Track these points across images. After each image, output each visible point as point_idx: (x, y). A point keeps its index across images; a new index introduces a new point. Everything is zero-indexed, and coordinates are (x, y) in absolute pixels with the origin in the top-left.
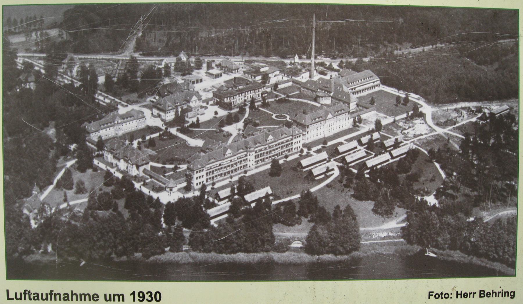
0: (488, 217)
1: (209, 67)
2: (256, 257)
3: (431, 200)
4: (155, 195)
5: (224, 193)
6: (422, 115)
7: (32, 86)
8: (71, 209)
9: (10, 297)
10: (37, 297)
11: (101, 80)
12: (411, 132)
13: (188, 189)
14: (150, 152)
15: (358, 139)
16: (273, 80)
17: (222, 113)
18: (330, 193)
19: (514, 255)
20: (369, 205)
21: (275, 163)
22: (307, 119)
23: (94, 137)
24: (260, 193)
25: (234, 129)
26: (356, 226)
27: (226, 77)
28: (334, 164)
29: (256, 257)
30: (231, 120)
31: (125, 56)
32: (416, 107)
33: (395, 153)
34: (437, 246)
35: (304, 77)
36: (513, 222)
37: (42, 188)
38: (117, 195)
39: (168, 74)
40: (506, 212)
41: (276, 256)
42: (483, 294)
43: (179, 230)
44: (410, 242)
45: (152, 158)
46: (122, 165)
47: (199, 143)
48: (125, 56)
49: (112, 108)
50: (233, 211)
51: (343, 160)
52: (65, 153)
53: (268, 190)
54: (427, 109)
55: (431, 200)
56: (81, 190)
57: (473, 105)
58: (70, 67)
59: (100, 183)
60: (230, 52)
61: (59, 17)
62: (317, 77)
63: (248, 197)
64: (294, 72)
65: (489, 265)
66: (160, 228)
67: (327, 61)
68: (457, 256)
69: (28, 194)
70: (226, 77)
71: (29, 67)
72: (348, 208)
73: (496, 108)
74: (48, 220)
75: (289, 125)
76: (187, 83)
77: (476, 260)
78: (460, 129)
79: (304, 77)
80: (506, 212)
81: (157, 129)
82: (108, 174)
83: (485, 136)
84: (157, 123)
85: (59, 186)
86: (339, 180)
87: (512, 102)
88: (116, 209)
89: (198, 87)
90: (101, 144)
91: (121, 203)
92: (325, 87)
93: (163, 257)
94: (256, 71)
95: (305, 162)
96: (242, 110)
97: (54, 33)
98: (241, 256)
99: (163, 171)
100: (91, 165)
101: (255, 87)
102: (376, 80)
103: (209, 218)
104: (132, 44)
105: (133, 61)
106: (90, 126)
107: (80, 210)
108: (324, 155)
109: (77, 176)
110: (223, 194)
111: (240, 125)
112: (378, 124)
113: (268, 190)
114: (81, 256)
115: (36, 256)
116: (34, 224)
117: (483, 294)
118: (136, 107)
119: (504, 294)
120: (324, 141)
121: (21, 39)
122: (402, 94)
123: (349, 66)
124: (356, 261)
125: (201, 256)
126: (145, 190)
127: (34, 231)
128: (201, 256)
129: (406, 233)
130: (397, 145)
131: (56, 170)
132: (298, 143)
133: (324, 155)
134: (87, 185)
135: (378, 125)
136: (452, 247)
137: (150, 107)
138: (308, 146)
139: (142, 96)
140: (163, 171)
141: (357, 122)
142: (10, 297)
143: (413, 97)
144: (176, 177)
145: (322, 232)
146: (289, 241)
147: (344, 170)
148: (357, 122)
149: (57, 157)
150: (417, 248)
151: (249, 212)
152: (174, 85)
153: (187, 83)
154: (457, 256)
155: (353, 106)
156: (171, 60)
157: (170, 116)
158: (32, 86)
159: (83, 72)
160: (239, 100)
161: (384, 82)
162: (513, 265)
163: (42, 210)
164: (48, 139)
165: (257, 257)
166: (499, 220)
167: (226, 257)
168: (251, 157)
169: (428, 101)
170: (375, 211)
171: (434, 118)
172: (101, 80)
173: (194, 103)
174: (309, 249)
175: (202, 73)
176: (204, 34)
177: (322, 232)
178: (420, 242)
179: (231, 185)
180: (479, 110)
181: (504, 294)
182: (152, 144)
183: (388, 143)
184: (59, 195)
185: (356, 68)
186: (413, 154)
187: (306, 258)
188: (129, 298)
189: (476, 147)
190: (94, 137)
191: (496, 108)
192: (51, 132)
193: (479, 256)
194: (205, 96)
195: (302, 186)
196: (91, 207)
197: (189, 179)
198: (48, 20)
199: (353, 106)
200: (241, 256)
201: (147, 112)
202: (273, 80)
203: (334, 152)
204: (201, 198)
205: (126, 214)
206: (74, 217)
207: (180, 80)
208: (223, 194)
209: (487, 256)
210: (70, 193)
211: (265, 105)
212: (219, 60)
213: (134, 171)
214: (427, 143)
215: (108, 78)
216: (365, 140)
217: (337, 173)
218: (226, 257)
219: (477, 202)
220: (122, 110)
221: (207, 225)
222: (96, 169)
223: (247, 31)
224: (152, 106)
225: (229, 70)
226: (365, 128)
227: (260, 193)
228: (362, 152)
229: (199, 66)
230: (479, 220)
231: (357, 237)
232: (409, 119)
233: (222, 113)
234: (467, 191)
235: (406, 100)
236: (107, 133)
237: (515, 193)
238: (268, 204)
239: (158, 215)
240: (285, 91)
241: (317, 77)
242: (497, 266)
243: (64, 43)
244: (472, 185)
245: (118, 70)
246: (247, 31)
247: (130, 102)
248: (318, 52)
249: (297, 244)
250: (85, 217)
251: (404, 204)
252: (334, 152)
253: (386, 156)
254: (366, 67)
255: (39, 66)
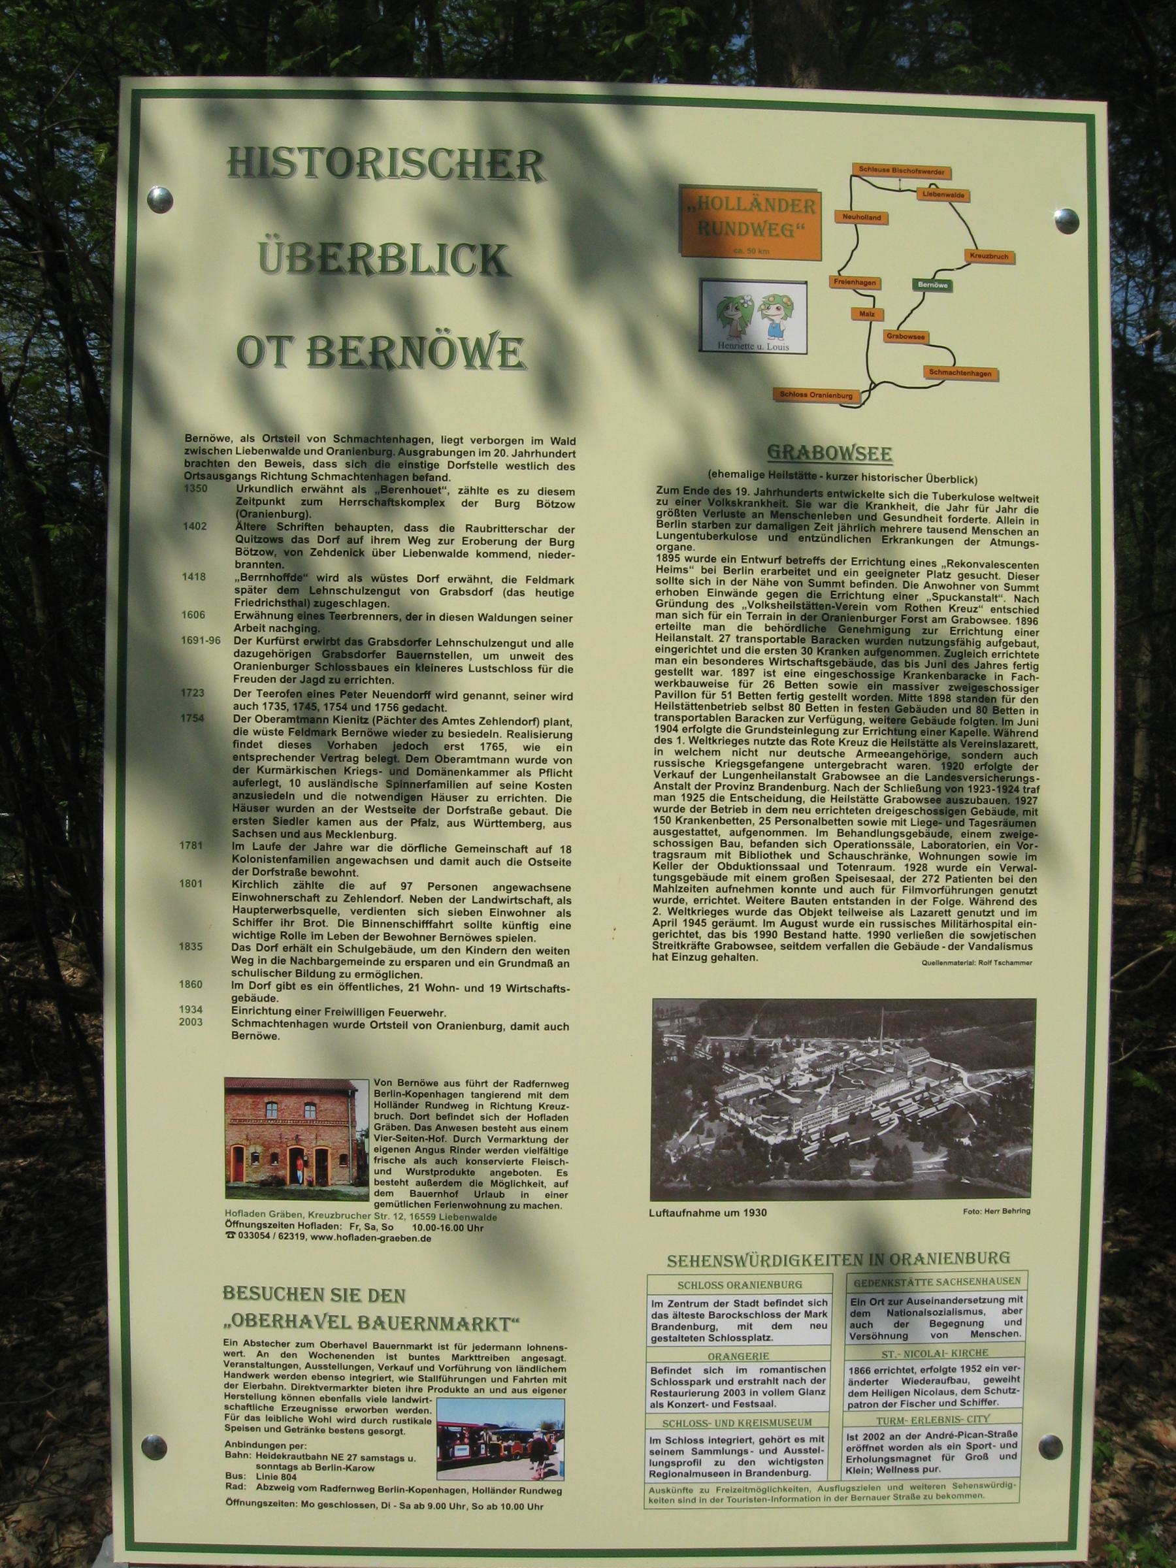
0: (1009, 1153)
1: (806, 1046)
2: (837, 1183)
3: (966, 1141)
4: (764, 1139)
5: (815, 1137)
6: (960, 1079)
7: (675, 1059)
8: (702, 1149)
9: (137, 1539)
10: (673, 1214)
11: (727, 1055)
12: (951, 1091)
13: (789, 1134)
14: (762, 1107)
15: (913, 1097)
16: (852, 1055)
17: (815, 1079)
18: (892, 1137)
19: (1029, 1182)
20: (921, 1145)
21: (852, 1115)
22: (876, 1083)
23: (721, 1096)
24: (841, 1137)
25: (823, 1091)
26: (910, 1160)
27: (818, 1053)
28: (895, 1116)
29: (837, 1183)
30: (821, 1084)
31: (745, 1038)
32: (956, 1073)
33: (940, 1107)
34: (970, 1175)
35: (874, 1053)
36: (1027, 1160)
37: (681, 1134)
38: (736, 1138)
39: (776, 1051)
40: (1023, 1150)
41: (851, 1182)
42: (1005, 1211)
43: (781, 1164)
44: (950, 1172)
45: (764, 1112)
46: (741, 1117)
47: (797, 1101)
48: (745, 1038)
49: (735, 1075)
50: (821, 1150)
51: (901, 1113)
52: (699, 1108)
53: (847, 1134)
54: (964, 1075)
55: (966, 1141)
56: (710, 1135)
57: (997, 1071)
58: (704, 1045)
59: (724, 1130)
60: (822, 1035)
61: (696, 1009)
62: (884, 1053)
63: (833, 1140)
64: (868, 1049)
65: (1006, 1187)
66: (767, 1162)
67: (891, 1041)
68: (986, 1182)
69: (670, 1138)
70: (818, 1053)
71: (672, 1045)
72: (905, 1149)
73: (1017, 1073)
74: (684, 1157)
75: (862, 1087)
76: (790, 1057)
77: (999, 1186)
78: (988, 1089)
79: (874, 1053)
80: (1023, 1150)
81: (766, 1091)
82: (731, 1123)
83: (1008, 1094)
84: (768, 1086)
85: (693, 1132)
86: (898, 1127)
87: (1029, 1069)
88: (735, 1148)
89: (798, 1060)
90: (726, 1102)
91: (740, 1144)
92: (889, 1060)
93: (769, 1184)
94: (840, 1049)
95: (873, 1114)
96: (829, 1077)
97: (692, 1020)
98: (826, 1182)
99: (771, 1121)
100: (718, 1117)
101: (839, 1060)
102: (927, 1054)
103: (804, 1155)
104: (751, 1029)
105: (751, 1042)
106: (718, 1089)
107: (709, 1150)
108: (888, 1109)
109: (707, 1125)
110: (814, 1137)
111: (828, 1087)
112: (928, 1086)
113: (847, 1134)
114: (708, 1183)
115: (674, 1184)
116: (673, 1160)
117: (1005, 1211)
118: (752, 1075)
119: (1022, 1211)
120: (888, 1099)
121: (667, 1024)
122: (946, 1064)
123: (907, 1044)
124: (910, 1186)
125: (797, 1182)
126: (758, 1135)
127: (674, 1166)
128: (797, 1182)
129: (946, 1165)
130: (941, 1101)
131: (692, 1121)
132: (869, 1100)
133: (888, 1109)
134: (715, 1131)
135: (928, 1087)
136: (983, 1175)
137: (763, 1075)
138: (877, 1103)
139: (757, 1067)
140: (771, 1121)
141: (913, 1085)
142: (137, 1539)
143: (954, 1066)
144: (781, 1125)
145: (885, 1164)
146: (861, 1171)
147: (902, 1119)
148: (913, 1085)
149: (693, 1111)
150: (955, 1176)
151: (833, 1150)
152: (781, 1059)
153: (790, 1057)
154: (986, 1182)
155: (909, 1073)
156: (778, 1041)
157: (777, 1081)
158: (675, 1059)
159: (714, 1049)
160: (827, 1069)
161: (933, 1056)
162: (1029, 1190)
163: (680, 1150)
164: (686, 1098)
165: (837, 1183)
166: (1018, 1156)
167: (815, 1183)
168: (835, 1110)
169: (965, 1069)
170: (925, 1149)
171: (969, 1081)
172: (727, 1055)
173: (795, 1072)
174: (875, 1176)
175: (801, 1050)
176: (803, 1022)
177: (885, 1164)
178: (957, 1172)
179: (820, 1131)
180: (1004, 1074)
181: (1022, 1211)
182: (763, 1101)
183: (934, 1100)
184: (694, 1139)
185: (913, 1046)
186: (953, 1107)
187: (873, 1183)
188: (742, 1213)
189: (1001, 1103)
190: (721, 1096)
191: (1017, 1073)
192: (689, 1092)
193: (1003, 1182)
194: (802, 1067)
195: (870, 1132)
196: (718, 1147)
197: (790, 1127)
198: (688, 1010)
199: (909, 1073)
200: (826, 1182)
201: (760, 1078)
202: (852, 1055)
203: (895, 1107)
204: (797, 1141)
205: (743, 1152)
206: (704, 1154)
207: (785, 1055)
208: (814, 1137)
209: (1009, 1183)
210: (702, 1137)
211: (846, 1073)
212: (813, 1041)
213: (750, 1121)
214: (963, 1100)
215: (732, 1054)
216: (918, 1098)
217: (896, 1122)
218: (815, 1183)
219: (1002, 1142)
220: (742, 1077)
221: (802, 1160)
222: (722, 1119)
223: (834, 1019)
224: (764, 1074)
225: (820, 1048)
226: (918, 1089)
227: (841, 1137)
228: (915, 1106)
229: (798, 1046)
230: (1003, 1155)
231: (911, 1168)
232: (951, 1082)
233: (815, 1079)
234: (993, 1134)
235: (949, 1068)
236: (730, 1094)
237: (1030, 1135)
238: (846, 1144)
239: (766, 1153)
240: (860, 1063)
241: (884, 1053)
242: (1016, 1190)
243: (700, 1027)
244: (998, 1131)
245: (740, 1047)
246: (834, 1019)
247: (748, 1071)
248: (885, 1035)
249: (867, 1174)
250: (713, 1155)
251: (946, 1144)
252: (895, 1107)
253: (933, 1110)
254: (920, 1045)
255: (681, 1044)
